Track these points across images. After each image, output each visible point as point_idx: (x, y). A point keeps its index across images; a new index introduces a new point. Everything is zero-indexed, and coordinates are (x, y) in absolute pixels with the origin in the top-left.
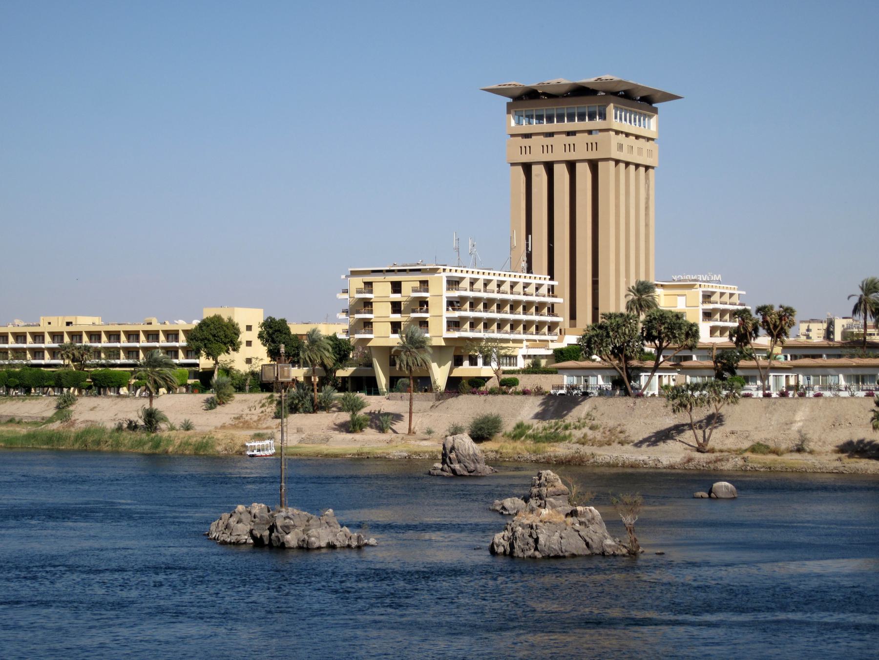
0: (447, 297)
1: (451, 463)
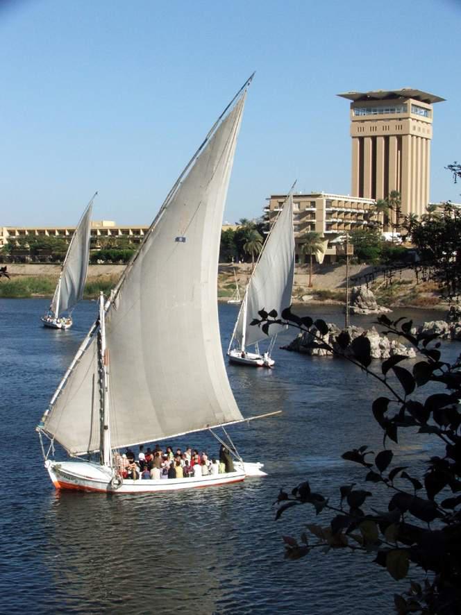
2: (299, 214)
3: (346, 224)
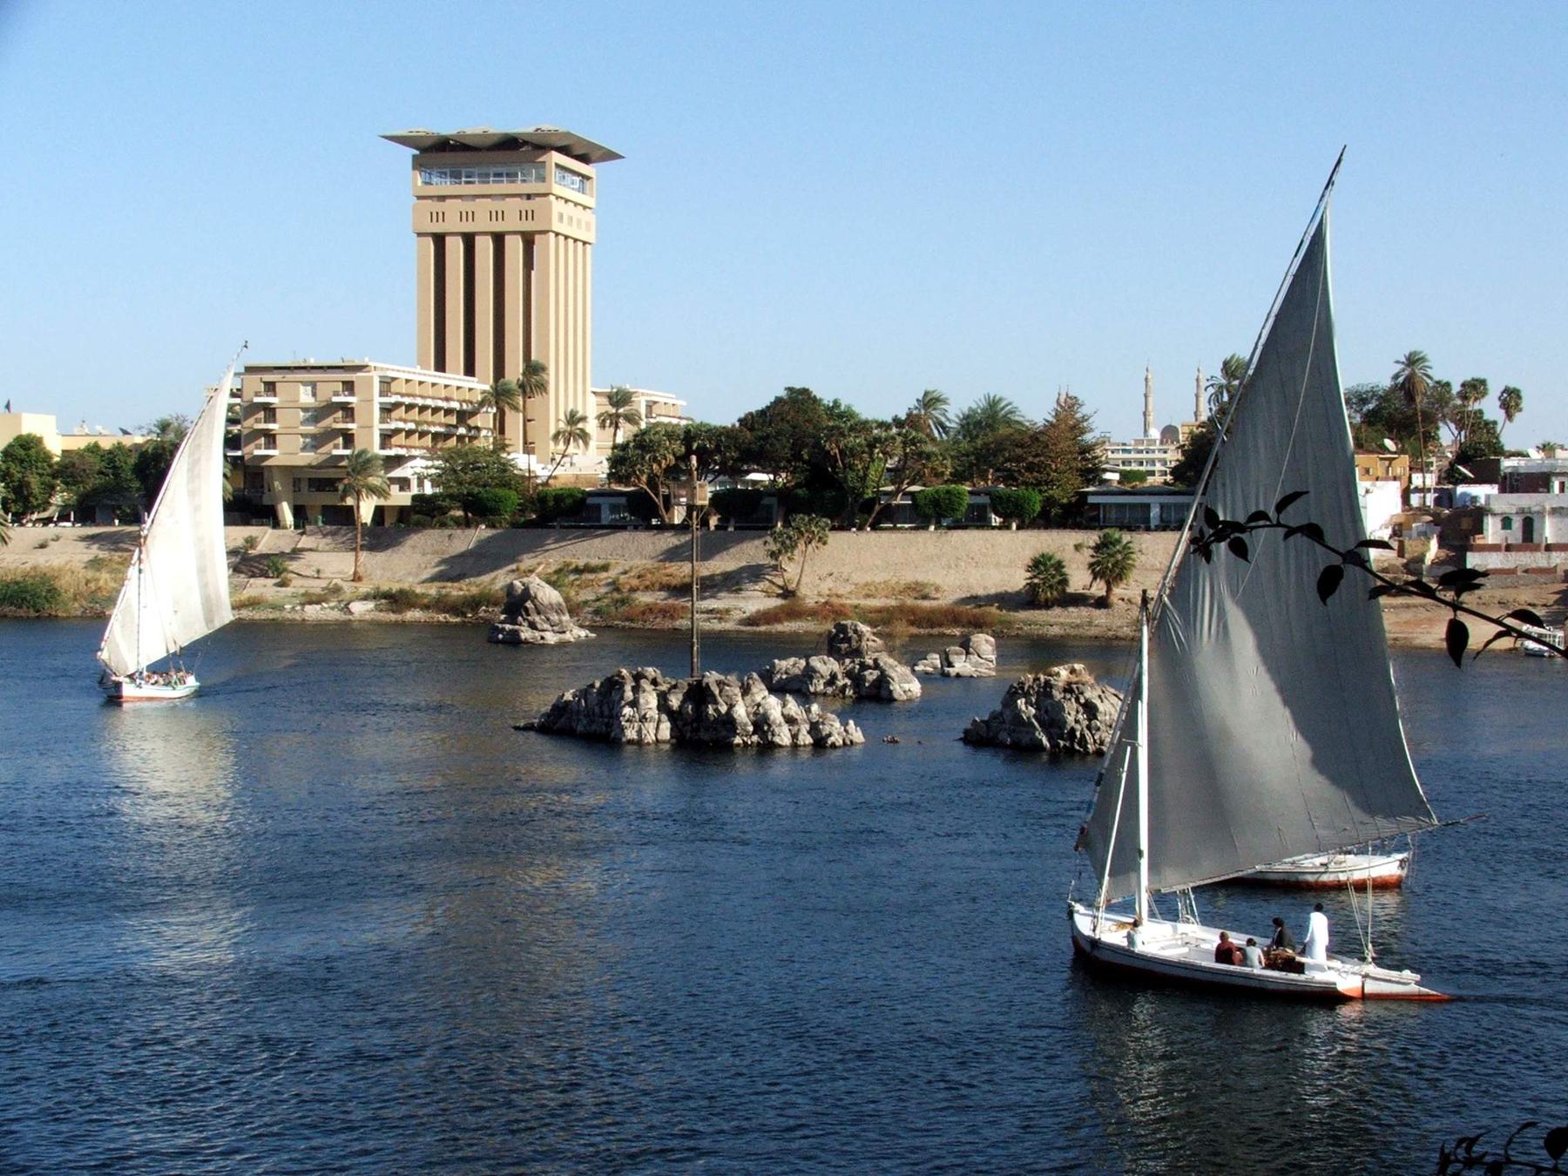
0: (380, 403)
1: (528, 615)
2: (316, 409)
3: (422, 434)
